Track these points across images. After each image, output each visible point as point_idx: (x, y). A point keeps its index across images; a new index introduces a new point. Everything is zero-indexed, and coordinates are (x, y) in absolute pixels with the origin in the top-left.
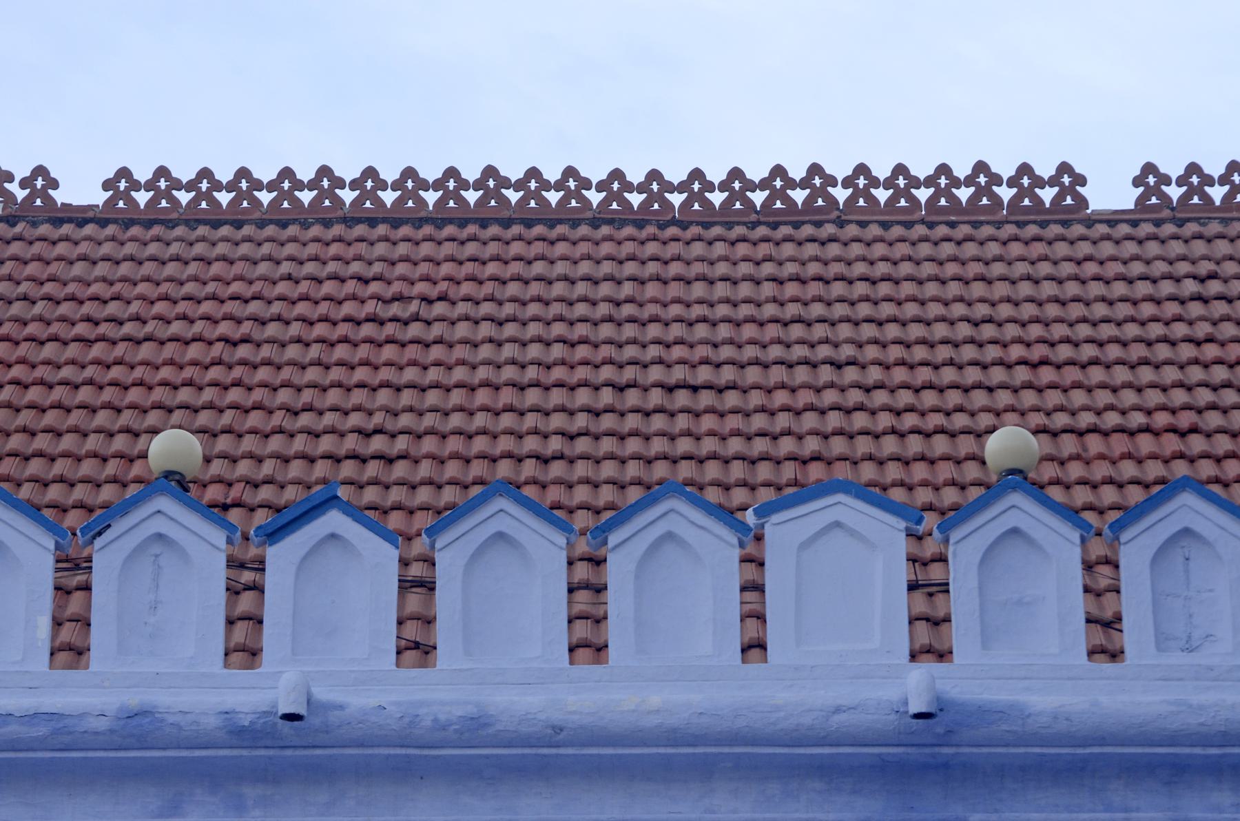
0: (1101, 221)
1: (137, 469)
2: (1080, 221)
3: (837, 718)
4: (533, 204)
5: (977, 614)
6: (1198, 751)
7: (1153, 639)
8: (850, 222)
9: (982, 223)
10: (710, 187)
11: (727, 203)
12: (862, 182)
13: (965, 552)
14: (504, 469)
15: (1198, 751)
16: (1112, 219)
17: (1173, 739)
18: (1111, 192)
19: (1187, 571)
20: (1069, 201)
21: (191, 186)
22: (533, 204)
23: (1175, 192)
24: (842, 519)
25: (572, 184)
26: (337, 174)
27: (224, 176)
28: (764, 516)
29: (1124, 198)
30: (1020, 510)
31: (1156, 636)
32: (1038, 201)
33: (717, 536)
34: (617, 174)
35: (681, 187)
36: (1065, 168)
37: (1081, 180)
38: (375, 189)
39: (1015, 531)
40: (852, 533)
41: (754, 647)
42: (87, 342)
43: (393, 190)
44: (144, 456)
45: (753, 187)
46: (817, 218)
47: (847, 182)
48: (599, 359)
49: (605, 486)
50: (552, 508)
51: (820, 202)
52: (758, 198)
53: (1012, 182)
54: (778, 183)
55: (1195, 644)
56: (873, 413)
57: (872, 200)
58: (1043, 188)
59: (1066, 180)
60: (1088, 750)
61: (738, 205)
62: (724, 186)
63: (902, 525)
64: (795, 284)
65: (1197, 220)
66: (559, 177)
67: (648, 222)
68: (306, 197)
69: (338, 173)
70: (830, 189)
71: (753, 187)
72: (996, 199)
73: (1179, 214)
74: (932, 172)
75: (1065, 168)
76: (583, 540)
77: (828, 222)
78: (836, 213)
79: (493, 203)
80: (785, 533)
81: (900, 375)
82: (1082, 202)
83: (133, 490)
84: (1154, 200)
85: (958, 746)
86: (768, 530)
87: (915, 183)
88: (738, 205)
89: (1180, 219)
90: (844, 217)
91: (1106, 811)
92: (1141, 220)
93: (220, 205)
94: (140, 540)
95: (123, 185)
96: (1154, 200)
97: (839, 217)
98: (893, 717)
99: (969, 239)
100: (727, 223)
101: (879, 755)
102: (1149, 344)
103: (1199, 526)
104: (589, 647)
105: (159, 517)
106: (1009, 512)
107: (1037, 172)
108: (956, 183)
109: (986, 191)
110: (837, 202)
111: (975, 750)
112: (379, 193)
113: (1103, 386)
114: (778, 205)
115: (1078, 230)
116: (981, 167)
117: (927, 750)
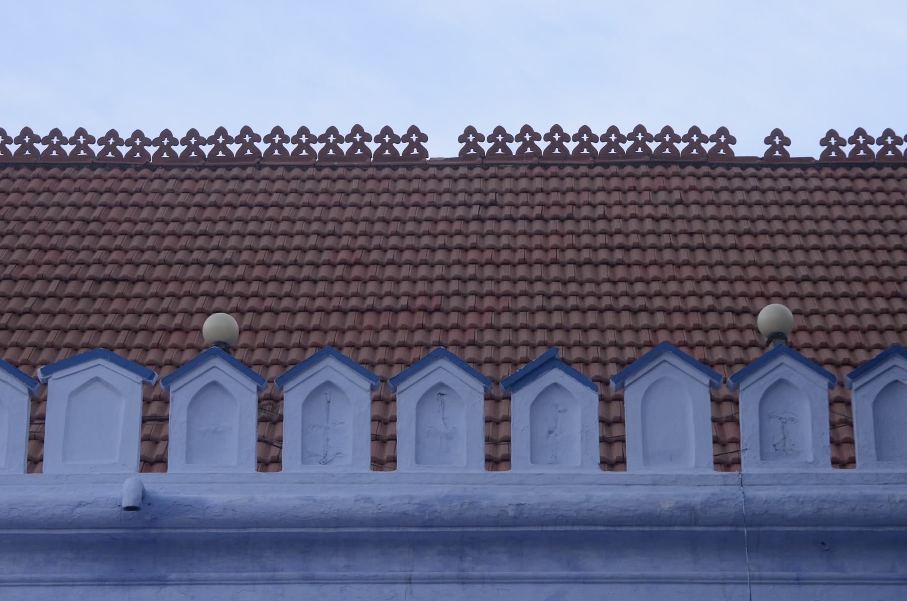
0: (433, 166)
1: (192, 338)
2: (419, 166)
3: (80, 510)
4: (54, 153)
5: (184, 440)
6: (320, 530)
7: (300, 455)
8: (265, 166)
9: (353, 167)
10: (174, 142)
11: (186, 153)
12: (277, 139)
13: (181, 397)
14: (105, 338)
15: (320, 530)
16: (805, 163)
17: (304, 522)
18: (443, 146)
19: (328, 410)
20: (415, 152)
21: (46, 141)
22: (54, 153)
23: (543, 145)
24: (101, 376)
25: (414, 138)
26: (89, 133)
27: (68, 134)
28: (47, 374)
29: (759, 150)
30: (219, 370)
31: (302, 453)
32: (395, 152)
33: (14, 388)
34: (278, 130)
35: (156, 142)
36: (413, 130)
37: (424, 138)
38: (169, 145)
39: (214, 384)
40: (107, 385)
41: (34, 462)
42: (43, 250)
43: (574, 141)
44: (199, 329)
45: (204, 142)
46: (244, 163)
47: (268, 139)
48: (548, 259)
49: (486, 347)
50: (362, 363)
51: (249, 152)
52: (207, 149)
53: (378, 139)
54: (221, 140)
55: (329, 459)
56: (667, 298)
57: (283, 151)
58: (398, 143)
59: (82, 140)
60: (248, 531)
61: (193, 155)
62: (185, 141)
63: (140, 379)
64: (587, 207)
65: (497, 165)
66: (295, 133)
67: (129, 166)
68: (234, 148)
69: (90, 132)
70: (255, 144)
71: (204, 142)
72: (367, 151)
73: (485, 161)
74: (324, 132)
75: (413, 130)
76: (270, 385)
77: (251, 166)
78: (258, 160)
79: (27, 153)
80: (61, 385)
81: (753, 272)
82: (424, 152)
83: (311, 352)
84: (472, 151)
85: (160, 528)
86: (50, 382)
87: (313, 139)
88: (193, 155)
89: (486, 164)
90: (262, 163)
91: (261, 571)
92: (460, 165)
93: (844, 154)
94: (881, 387)
95: (277, 139)
96: (472, 151)
97: (258, 163)
98: (116, 509)
99: (890, 177)
100: (182, 167)
101: (108, 535)
102: (890, 251)
103: (337, 380)
104: (269, 460)
105: (214, 370)
106: (211, 371)
107: (676, 132)
108: (340, 139)
109: (360, 145)
110: (260, 153)
111: (172, 531)
112: (173, 147)
113: (857, 279)
114: (220, 154)
115: (417, 171)
116: (357, 129)
117: (141, 531)
